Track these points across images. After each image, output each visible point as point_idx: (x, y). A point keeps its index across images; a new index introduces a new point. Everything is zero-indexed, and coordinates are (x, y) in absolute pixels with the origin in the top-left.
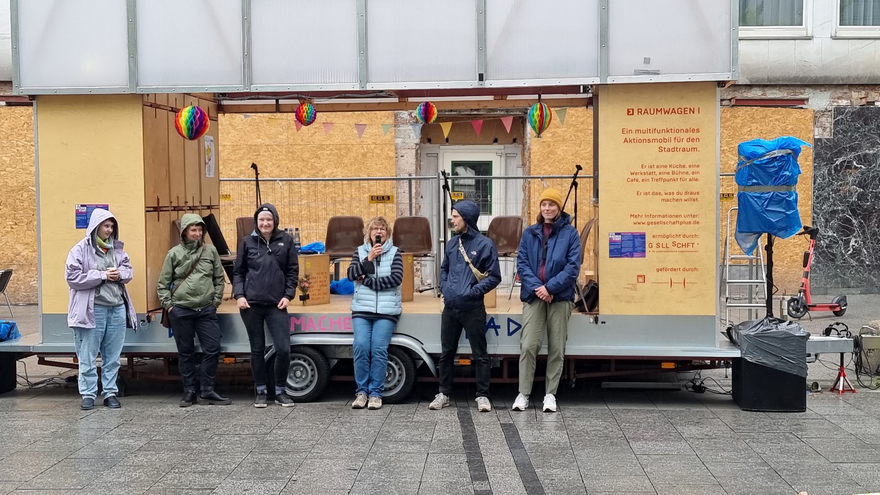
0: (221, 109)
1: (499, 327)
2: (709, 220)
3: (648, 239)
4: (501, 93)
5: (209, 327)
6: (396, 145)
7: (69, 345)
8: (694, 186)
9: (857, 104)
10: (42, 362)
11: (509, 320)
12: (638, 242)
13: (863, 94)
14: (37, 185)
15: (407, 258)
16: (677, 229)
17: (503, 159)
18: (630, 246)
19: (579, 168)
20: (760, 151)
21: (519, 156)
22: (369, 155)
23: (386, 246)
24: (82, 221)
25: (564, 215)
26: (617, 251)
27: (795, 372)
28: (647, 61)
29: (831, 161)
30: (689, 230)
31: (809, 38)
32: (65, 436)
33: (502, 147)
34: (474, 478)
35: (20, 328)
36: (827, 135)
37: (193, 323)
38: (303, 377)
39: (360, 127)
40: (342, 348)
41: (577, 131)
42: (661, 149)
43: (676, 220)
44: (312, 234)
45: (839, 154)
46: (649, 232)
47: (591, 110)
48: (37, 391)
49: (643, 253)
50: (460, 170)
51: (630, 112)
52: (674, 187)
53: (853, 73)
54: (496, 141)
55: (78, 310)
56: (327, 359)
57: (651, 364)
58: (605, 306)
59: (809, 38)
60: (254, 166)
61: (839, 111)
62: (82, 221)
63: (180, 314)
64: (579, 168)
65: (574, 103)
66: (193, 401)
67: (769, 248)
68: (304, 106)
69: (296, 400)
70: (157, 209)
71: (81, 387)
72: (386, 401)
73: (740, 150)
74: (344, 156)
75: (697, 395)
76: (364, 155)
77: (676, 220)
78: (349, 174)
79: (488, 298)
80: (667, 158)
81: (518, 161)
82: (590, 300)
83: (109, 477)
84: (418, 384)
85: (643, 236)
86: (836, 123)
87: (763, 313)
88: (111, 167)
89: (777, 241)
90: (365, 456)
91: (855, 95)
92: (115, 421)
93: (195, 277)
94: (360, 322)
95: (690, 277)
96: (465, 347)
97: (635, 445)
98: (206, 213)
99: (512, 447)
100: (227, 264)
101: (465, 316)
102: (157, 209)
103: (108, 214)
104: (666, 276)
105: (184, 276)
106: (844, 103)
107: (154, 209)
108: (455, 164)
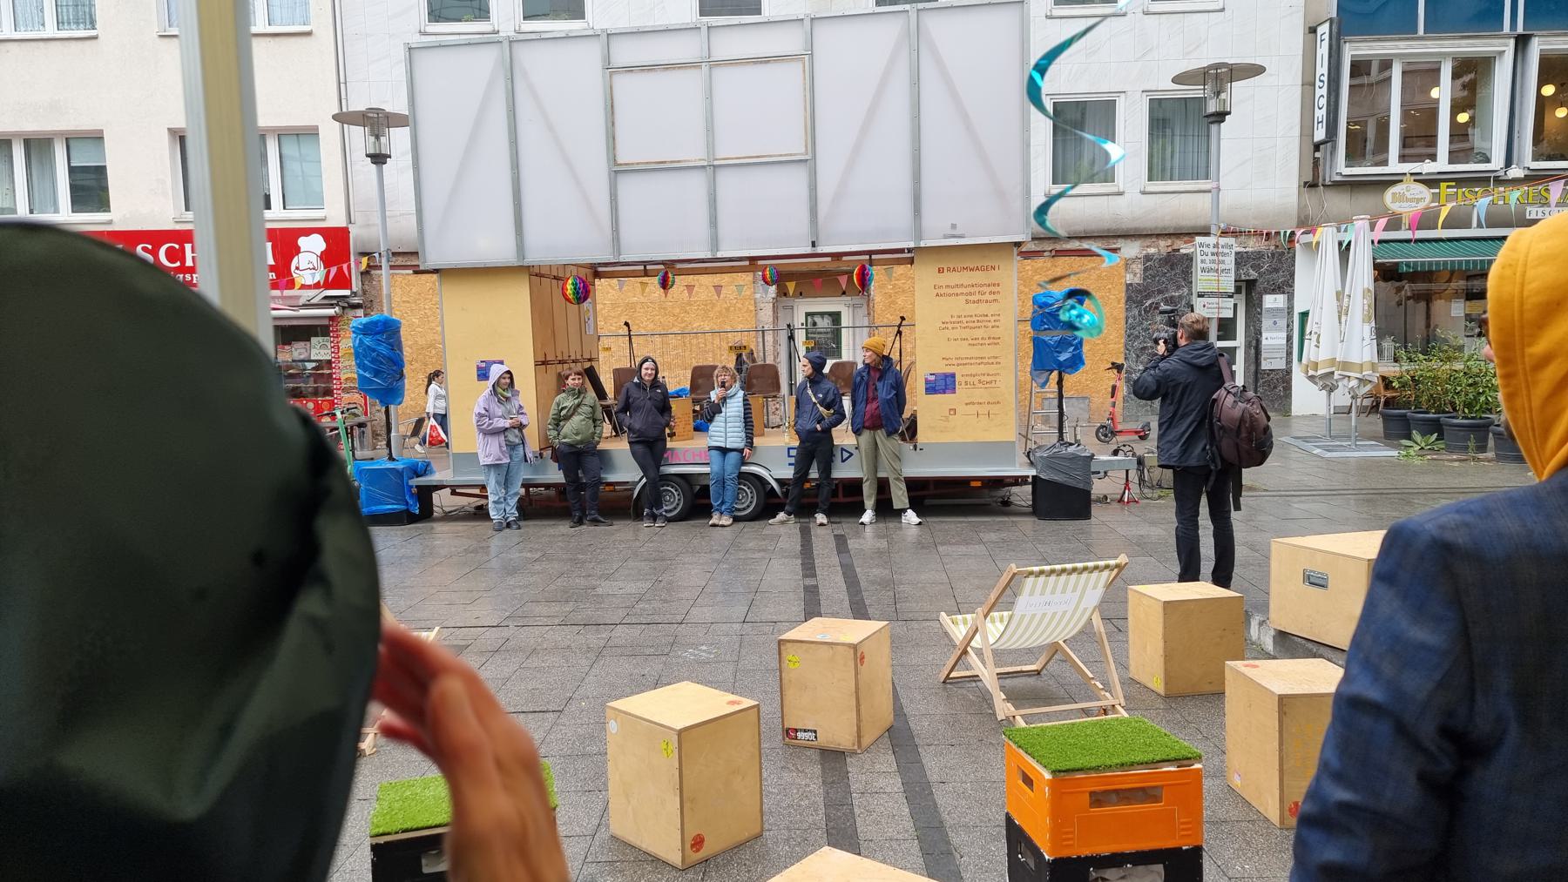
0: (597, 275)
2: (1009, 360)
3: (958, 378)
4: (837, 256)
5: (592, 462)
7: (479, 478)
8: (996, 332)
9: (1164, 251)
10: (454, 493)
12: (949, 380)
13: (1169, 242)
14: (443, 343)
15: (757, 401)
16: (982, 369)
18: (942, 384)
19: (903, 318)
20: (1051, 301)
23: (731, 391)
24: (483, 374)
25: (887, 359)
26: (931, 389)
27: (1081, 486)
28: (954, 226)
29: (1140, 303)
30: (992, 369)
31: (1120, 194)
32: (475, 551)
34: (805, 576)
35: (434, 466)
36: (1137, 280)
37: (578, 458)
38: (674, 500)
39: (718, 288)
42: (967, 302)
43: (981, 360)
44: (676, 380)
45: (1147, 297)
46: (959, 372)
48: (448, 517)
49: (953, 390)
50: (818, 319)
51: (940, 271)
52: (979, 333)
53: (1160, 224)
55: (489, 451)
56: (691, 486)
57: (961, 484)
58: (922, 436)
59: (1120, 194)
60: (627, 324)
61: (1148, 258)
62: (483, 374)
63: (567, 450)
64: (903, 318)
65: (899, 262)
66: (580, 522)
67: (1060, 383)
68: (667, 273)
69: (670, 520)
70: (544, 363)
71: (492, 513)
72: (736, 519)
73: (1035, 300)
75: (1005, 507)
76: (727, 309)
77: (981, 360)
79: (835, 432)
80: (973, 309)
81: (864, 310)
82: (912, 430)
83: (511, 581)
84: (769, 503)
85: (953, 376)
86: (1146, 270)
87: (1054, 439)
88: (503, 329)
89: (1066, 377)
90: (719, 562)
91: (1162, 243)
92: (516, 540)
93: (576, 418)
94: (714, 453)
95: (994, 409)
96: (814, 474)
97: (940, 549)
98: (587, 365)
99: (839, 552)
100: (607, 410)
101: (815, 447)
102: (544, 363)
103: (504, 368)
104: (973, 409)
105: (567, 418)
106: (1152, 251)
107: (542, 363)
108: (807, 314)
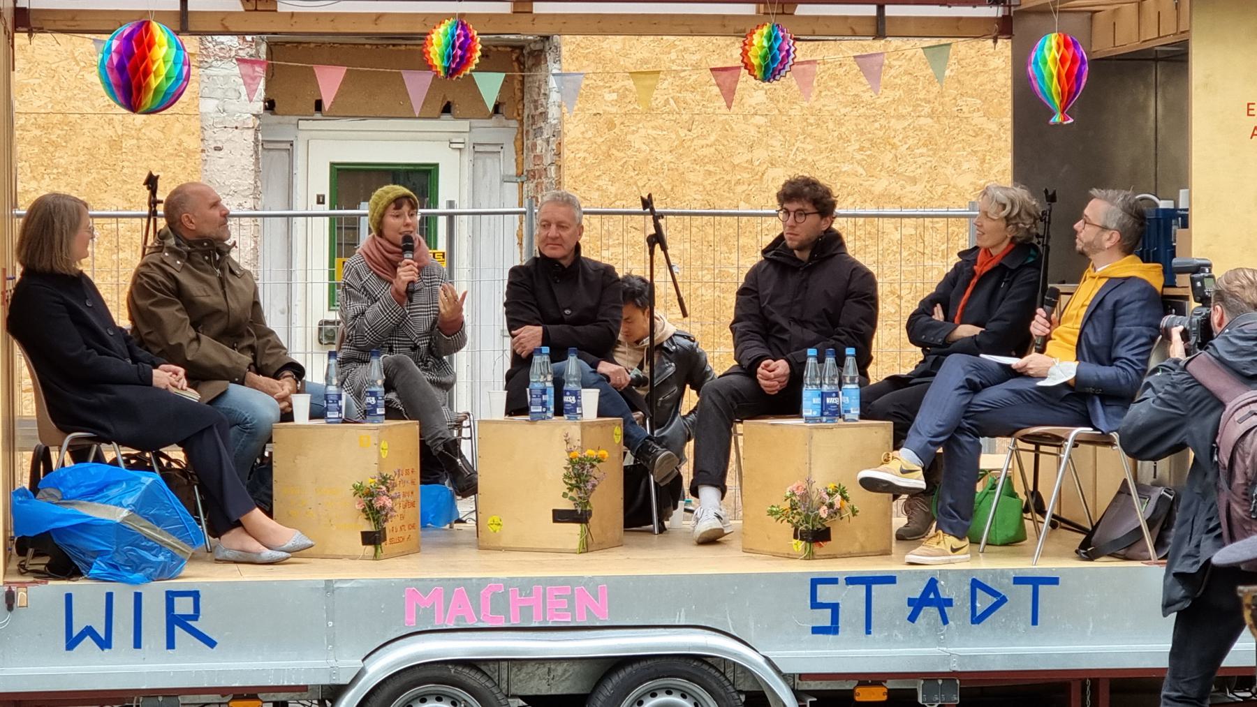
1: (949, 602)
6: (201, 117)
11: (976, 584)
17: (467, 157)
21: (510, 150)
22: (129, 143)
33: (464, 125)
40: (529, 668)
41: (682, 89)
47: (1005, 46)
54: (447, 109)
74: (57, 146)
78: (694, 204)
